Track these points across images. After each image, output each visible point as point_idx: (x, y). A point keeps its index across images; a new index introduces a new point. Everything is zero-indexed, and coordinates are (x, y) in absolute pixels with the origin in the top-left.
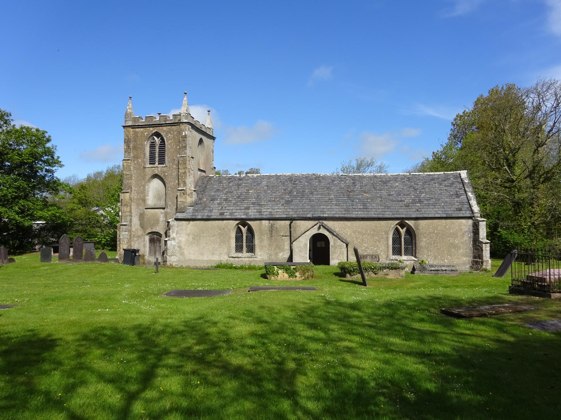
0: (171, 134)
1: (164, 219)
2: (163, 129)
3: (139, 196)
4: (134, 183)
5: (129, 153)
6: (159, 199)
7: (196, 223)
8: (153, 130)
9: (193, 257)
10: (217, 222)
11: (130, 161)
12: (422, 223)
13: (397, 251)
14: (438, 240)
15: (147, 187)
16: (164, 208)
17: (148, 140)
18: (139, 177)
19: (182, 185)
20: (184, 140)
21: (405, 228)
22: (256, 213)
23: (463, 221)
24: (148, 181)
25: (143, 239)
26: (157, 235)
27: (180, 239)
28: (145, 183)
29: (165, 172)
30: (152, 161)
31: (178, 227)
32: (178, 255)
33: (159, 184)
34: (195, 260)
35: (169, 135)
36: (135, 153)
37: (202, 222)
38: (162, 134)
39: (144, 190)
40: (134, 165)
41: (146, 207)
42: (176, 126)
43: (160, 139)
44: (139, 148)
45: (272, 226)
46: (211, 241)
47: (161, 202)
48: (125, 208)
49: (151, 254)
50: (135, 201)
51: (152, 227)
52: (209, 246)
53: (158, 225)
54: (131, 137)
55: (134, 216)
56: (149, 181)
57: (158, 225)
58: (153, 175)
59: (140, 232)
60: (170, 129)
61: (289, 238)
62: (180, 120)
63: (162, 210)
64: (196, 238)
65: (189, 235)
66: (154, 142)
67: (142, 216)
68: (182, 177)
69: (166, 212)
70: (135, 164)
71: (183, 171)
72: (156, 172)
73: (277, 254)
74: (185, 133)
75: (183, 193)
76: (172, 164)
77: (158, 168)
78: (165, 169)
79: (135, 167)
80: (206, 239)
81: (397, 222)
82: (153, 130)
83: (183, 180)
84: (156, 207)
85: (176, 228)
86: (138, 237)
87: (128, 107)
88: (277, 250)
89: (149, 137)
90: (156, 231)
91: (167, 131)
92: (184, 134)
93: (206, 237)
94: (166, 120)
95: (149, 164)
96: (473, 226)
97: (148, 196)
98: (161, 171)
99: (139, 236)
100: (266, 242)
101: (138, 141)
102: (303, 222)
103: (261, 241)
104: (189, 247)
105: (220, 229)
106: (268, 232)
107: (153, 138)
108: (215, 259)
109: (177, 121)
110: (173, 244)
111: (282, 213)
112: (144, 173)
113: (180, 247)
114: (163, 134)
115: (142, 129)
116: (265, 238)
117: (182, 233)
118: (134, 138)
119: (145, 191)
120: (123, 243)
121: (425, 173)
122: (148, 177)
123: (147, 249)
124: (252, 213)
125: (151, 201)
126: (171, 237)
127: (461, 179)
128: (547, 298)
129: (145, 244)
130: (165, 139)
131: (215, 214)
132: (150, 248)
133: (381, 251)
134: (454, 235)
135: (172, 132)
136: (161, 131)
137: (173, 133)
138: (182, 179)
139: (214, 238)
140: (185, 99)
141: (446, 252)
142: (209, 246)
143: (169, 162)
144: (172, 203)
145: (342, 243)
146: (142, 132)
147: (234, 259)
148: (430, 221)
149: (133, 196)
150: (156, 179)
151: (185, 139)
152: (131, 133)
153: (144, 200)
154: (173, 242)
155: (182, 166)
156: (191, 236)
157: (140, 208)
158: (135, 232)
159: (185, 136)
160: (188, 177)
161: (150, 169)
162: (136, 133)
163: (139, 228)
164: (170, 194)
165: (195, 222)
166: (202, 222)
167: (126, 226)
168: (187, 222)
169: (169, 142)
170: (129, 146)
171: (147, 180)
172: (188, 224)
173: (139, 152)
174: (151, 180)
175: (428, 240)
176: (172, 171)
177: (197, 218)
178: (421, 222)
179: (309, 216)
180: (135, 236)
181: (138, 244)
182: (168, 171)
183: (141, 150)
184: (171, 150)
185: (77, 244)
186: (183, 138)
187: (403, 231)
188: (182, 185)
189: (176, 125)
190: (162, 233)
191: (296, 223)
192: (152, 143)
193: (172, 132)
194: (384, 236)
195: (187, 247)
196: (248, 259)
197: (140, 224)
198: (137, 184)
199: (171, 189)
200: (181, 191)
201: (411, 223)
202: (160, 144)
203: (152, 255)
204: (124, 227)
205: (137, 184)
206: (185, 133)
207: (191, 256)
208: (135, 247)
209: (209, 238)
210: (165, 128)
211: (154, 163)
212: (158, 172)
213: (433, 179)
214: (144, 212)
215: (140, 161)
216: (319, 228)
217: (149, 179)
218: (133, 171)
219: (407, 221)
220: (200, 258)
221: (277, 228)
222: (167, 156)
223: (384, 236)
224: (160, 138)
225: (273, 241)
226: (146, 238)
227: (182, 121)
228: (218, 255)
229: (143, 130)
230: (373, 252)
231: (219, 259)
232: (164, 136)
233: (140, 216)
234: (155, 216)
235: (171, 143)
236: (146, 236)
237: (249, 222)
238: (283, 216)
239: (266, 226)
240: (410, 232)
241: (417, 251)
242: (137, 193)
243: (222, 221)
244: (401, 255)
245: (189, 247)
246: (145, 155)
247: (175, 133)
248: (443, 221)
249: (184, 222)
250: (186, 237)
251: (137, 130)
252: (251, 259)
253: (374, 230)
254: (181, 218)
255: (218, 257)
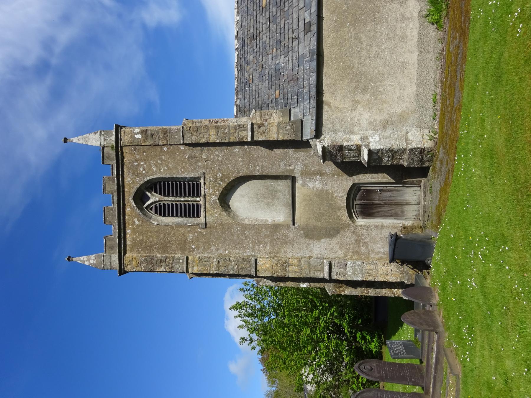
0: (139, 165)
1: (318, 177)
2: (129, 184)
3: (267, 240)
4: (237, 251)
5: (175, 261)
6: (273, 195)
7: (328, 85)
8: (130, 203)
9: (411, 90)
10: (325, 33)
15: (246, 222)
16: (294, 180)
17: (151, 218)
18: (224, 239)
24: (233, 218)
25: (364, 232)
26: (354, 199)
27: (364, 123)
28: (238, 224)
29: (216, 178)
31: (336, 131)
32: (405, 129)
33: (242, 196)
34: (418, 85)
35: (141, 169)
36: (174, 247)
37: (324, 71)
38: (138, 186)
39: (252, 227)
40: (201, 250)
41: (291, 223)
42: (124, 155)
43: (150, 192)
44: (164, 237)
46: (371, 46)
47: (280, 191)
48: (291, 268)
49: (399, 212)
50: (276, 249)
51: (335, 209)
52: (383, 51)
54: (141, 256)
55: (311, 251)
56: (234, 216)
57: (332, 193)
58: (222, 207)
59: (348, 237)
60: (129, 168)
62: (112, 147)
63: (298, 184)
65: (356, 103)
68: (225, 133)
69: (302, 174)
71: (213, 132)
72: (215, 198)
74: (138, 133)
75: (260, 127)
76: (198, 161)
78: (209, 178)
79: (205, 248)
80: (365, 59)
82: (130, 203)
83: (232, 131)
85: (340, 135)
86: (358, 241)
89: (145, 215)
90: (345, 198)
91: (133, 174)
92: (139, 136)
93: (361, 57)
95: (199, 219)
97: (267, 220)
98: (213, 187)
99: (357, 240)
101: (151, 239)
104: (385, 102)
105: (343, 24)
107: (147, 208)
108: (415, 32)
110: (378, 139)
113: (385, 125)
114: (139, 182)
115: (128, 231)
117: (351, 119)
119: (254, 225)
120: (374, 273)
122: (225, 217)
123: (388, 222)
126: (359, 142)
129: (376, 226)
130: (149, 178)
132: (384, 216)
135: (135, 164)
136: (133, 188)
137: (136, 161)
138: (230, 134)
140: (75, 140)
142: (383, 51)
143: (195, 169)
144: (282, 159)
146: (134, 231)
149: (266, 253)
150: (230, 203)
152: (135, 255)
153: (276, 227)
154: (371, 140)
155: (201, 135)
156: (358, 98)
157: (291, 236)
158: (348, 250)
160: (227, 123)
162: (135, 245)
163: (337, 239)
164: (262, 165)
165: (325, 87)
166: (325, 70)
167: (333, 265)
168: (325, 108)
169: (155, 169)
170: (161, 261)
172: (329, 106)
173: (174, 239)
174: (231, 214)
176: (213, 162)
177: (315, 83)
180: (357, 249)
181: (375, 243)
182: (213, 170)
183: (169, 234)
184: (170, 165)
185: (379, 373)
190: (350, 184)
192: (156, 212)
193: (135, 164)
195: (386, 106)
197: (329, 237)
198: (239, 244)
199: (253, 163)
200: (256, 133)
202: (160, 194)
203: (403, 212)
205: (239, 244)
206: (138, 133)
207: (409, 95)
208: (382, 250)
209: (365, 52)
210: (128, 180)
211: (198, 205)
212: (214, 193)
215: (191, 236)
217: (229, 215)
218: (212, 252)
220: (413, 70)
222: (183, 173)
224: (147, 193)
226: (361, 224)
228: (407, 25)
229: (130, 229)
231: (416, 20)
232: (142, 182)
234: (311, 200)
235: (156, 165)
236: (357, 224)
243: (324, 21)
245: (385, 102)
246: (178, 225)
247: (138, 157)
249: (325, 116)
250: (360, 108)
251: (128, 242)
254: (314, 122)
255: (411, 25)
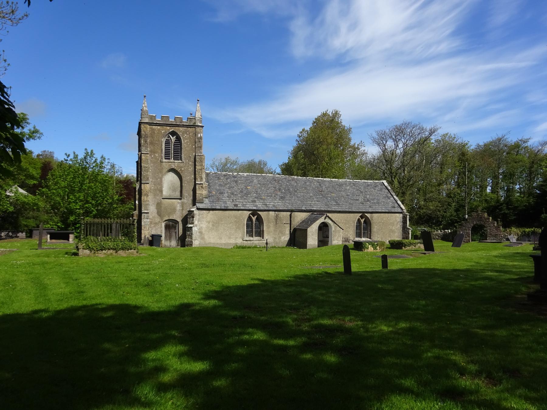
0: (187, 134)
2: (179, 129)
5: (146, 148)
6: (174, 190)
11: (148, 155)
12: (375, 215)
13: (359, 235)
14: (383, 227)
15: (163, 179)
19: (199, 180)
20: (200, 141)
21: (364, 219)
22: (263, 206)
23: (398, 215)
27: (202, 225)
29: (181, 167)
30: (167, 156)
33: (174, 177)
34: (214, 243)
35: (186, 135)
36: (152, 148)
38: (178, 133)
41: (163, 198)
43: (176, 138)
45: (277, 216)
46: (228, 228)
51: (169, 215)
52: (226, 231)
53: (175, 214)
57: (175, 214)
59: (158, 219)
60: (186, 130)
61: (289, 225)
62: (195, 123)
63: (179, 201)
64: (215, 225)
66: (169, 140)
67: (159, 206)
68: (199, 172)
69: (182, 202)
70: (152, 158)
71: (200, 168)
72: (173, 167)
73: (280, 237)
74: (200, 135)
75: (201, 187)
76: (188, 160)
77: (176, 164)
78: (182, 165)
79: (152, 161)
81: (250, 212)
83: (200, 175)
84: (171, 198)
85: (198, 217)
86: (156, 223)
87: (144, 105)
88: (280, 235)
89: (166, 135)
91: (184, 132)
92: (199, 136)
94: (181, 122)
96: (403, 218)
98: (177, 166)
100: (272, 229)
101: (155, 137)
102: (299, 213)
103: (269, 227)
106: (274, 221)
108: (231, 242)
109: (192, 124)
111: (283, 206)
112: (161, 166)
114: (180, 134)
115: (159, 127)
116: (272, 225)
117: (203, 221)
118: (151, 134)
121: (362, 181)
124: (260, 205)
125: (166, 192)
126: (195, 224)
127: (385, 186)
128: (67, 241)
129: (162, 230)
130: (182, 138)
131: (230, 205)
132: (165, 233)
133: (350, 234)
134: (393, 224)
137: (189, 133)
139: (231, 225)
141: (388, 235)
142: (226, 231)
144: (188, 194)
145: (340, 229)
146: (159, 130)
147: (247, 242)
148: (379, 214)
150: (171, 172)
151: (201, 140)
153: (161, 191)
154: (196, 228)
159: (201, 138)
161: (167, 164)
163: (156, 215)
168: (208, 212)
171: (164, 173)
172: (208, 213)
173: (156, 148)
175: (378, 227)
176: (188, 166)
178: (374, 214)
179: (303, 208)
180: (153, 223)
181: (155, 230)
184: (187, 148)
186: (198, 139)
187: (254, 219)
188: (199, 180)
189: (192, 127)
191: (294, 214)
192: (166, 140)
194: (352, 224)
196: (258, 242)
201: (368, 215)
203: (167, 240)
204: (145, 214)
206: (200, 135)
210: (181, 129)
213: (368, 185)
214: (161, 202)
215: (157, 155)
216: (325, 218)
219: (366, 214)
221: (280, 218)
222: (184, 154)
223: (352, 224)
225: (277, 227)
227: (196, 124)
230: (345, 236)
231: (235, 242)
232: (180, 136)
233: (157, 205)
235: (187, 142)
237: (259, 213)
238: (285, 208)
239: (272, 216)
240: (368, 223)
241: (372, 235)
242: (154, 184)
244: (361, 238)
245: (209, 232)
247: (191, 134)
248: (387, 214)
249: (205, 211)
251: (154, 127)
252: (260, 242)
253: (346, 220)
255: (234, 240)
